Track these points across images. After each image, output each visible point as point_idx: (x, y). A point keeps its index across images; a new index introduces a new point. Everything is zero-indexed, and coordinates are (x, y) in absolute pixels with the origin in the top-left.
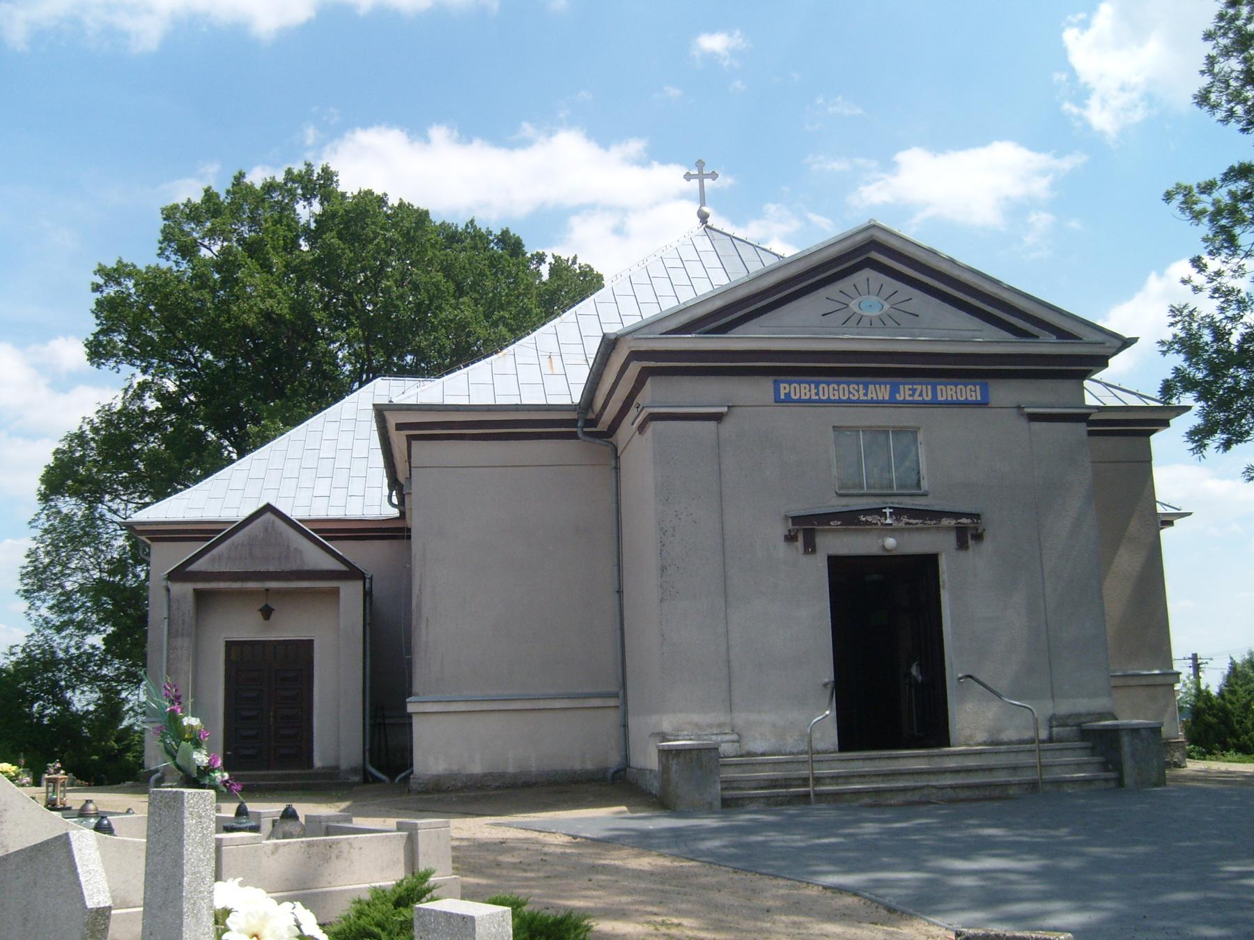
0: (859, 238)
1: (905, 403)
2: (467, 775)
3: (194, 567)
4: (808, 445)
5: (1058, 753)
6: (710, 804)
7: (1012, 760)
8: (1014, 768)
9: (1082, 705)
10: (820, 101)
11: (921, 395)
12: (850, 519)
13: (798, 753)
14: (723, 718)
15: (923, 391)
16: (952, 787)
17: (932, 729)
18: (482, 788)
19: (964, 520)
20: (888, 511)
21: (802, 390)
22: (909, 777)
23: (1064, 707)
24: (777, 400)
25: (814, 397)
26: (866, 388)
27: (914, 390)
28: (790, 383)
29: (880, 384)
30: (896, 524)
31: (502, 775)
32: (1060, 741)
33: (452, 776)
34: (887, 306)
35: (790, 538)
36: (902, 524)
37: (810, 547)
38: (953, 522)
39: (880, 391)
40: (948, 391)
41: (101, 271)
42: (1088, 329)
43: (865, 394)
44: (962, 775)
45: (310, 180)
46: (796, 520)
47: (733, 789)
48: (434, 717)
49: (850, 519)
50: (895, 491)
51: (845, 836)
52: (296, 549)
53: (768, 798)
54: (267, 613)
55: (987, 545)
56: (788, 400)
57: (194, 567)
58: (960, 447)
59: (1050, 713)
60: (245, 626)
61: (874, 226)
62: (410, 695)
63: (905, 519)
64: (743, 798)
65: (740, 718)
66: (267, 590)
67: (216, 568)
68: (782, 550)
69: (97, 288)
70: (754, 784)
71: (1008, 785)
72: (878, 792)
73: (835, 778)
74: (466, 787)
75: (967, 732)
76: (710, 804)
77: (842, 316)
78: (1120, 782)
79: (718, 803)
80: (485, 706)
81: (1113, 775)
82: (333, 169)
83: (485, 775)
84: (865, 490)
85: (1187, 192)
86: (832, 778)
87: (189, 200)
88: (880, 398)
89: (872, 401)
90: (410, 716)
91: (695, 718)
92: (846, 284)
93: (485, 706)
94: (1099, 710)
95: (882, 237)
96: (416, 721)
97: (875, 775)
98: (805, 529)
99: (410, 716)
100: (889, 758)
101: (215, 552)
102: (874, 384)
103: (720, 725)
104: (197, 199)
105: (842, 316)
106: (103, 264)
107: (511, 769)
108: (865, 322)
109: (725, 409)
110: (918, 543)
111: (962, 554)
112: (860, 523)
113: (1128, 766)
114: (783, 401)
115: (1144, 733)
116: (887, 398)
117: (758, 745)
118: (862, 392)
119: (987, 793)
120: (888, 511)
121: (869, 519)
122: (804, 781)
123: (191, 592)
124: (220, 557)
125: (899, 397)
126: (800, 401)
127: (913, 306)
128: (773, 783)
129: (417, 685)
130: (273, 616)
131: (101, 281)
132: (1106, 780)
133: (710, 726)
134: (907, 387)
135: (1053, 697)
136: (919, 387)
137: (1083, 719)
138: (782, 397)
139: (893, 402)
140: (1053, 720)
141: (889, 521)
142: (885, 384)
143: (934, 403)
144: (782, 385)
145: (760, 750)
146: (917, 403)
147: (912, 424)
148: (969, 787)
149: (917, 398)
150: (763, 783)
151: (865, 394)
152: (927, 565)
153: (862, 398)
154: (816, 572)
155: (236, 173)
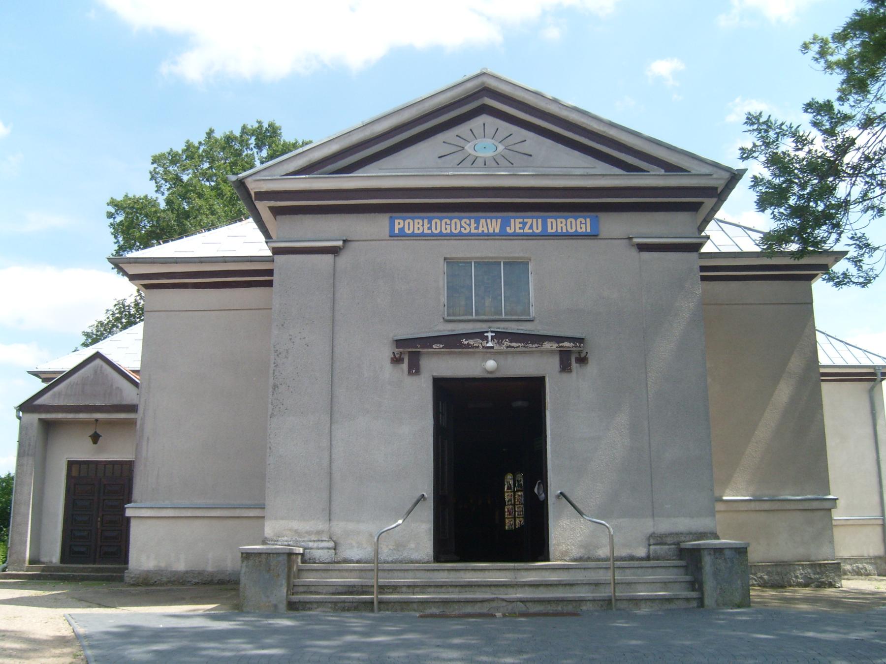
0: (470, 85)
1: (515, 236)
2: (171, 572)
3: (39, 402)
4: (408, 273)
5: (650, 570)
6: (276, 606)
7: (593, 576)
8: (597, 584)
9: (682, 524)
10: (738, 100)
11: (531, 227)
12: (452, 342)
13: (392, 562)
14: (321, 525)
15: (534, 224)
16: (523, 601)
17: (531, 543)
18: (183, 583)
19: (566, 344)
20: (490, 335)
21: (415, 225)
22: (488, 589)
23: (665, 526)
24: (392, 235)
25: (426, 231)
26: (477, 222)
27: (525, 224)
28: (404, 219)
29: (491, 219)
30: (497, 347)
31: (200, 573)
32: (658, 559)
33: (159, 572)
34: (501, 148)
35: (396, 360)
36: (503, 348)
37: (414, 368)
38: (555, 345)
39: (491, 224)
40: (558, 224)
41: (113, 203)
42: (696, 162)
43: (477, 228)
44: (541, 588)
45: (260, 133)
46: (399, 343)
47: (311, 593)
48: (149, 521)
49: (452, 342)
50: (503, 317)
51: (777, 635)
52: (118, 388)
53: (335, 603)
54: (95, 438)
55: (591, 368)
56: (402, 235)
57: (39, 402)
58: (570, 275)
59: (650, 530)
60: (82, 450)
61: (484, 74)
62: (129, 501)
63: (506, 343)
64: (311, 603)
65: (339, 527)
66: (97, 420)
67: (56, 403)
68: (388, 371)
69: (110, 215)
70: (331, 590)
71: (581, 601)
72: (445, 602)
73: (412, 587)
74: (170, 582)
75: (563, 548)
76: (276, 606)
77: (458, 157)
78: (701, 601)
79: (283, 606)
80: (189, 513)
81: (694, 594)
82: (277, 125)
83: (187, 572)
84: (474, 317)
85: (824, 42)
86: (409, 586)
87: (171, 150)
88: (491, 231)
89: (483, 235)
90: (128, 519)
91: (295, 525)
92: (463, 129)
93: (189, 513)
94: (702, 530)
95: (493, 84)
96: (133, 523)
97: (451, 586)
98: (410, 352)
99: (128, 519)
100: (474, 570)
101: (56, 389)
102: (486, 218)
103: (318, 533)
104: (179, 148)
105: (458, 157)
106: (115, 197)
107: (210, 569)
108: (480, 162)
109: (340, 243)
110: (522, 365)
111: (565, 376)
112: (462, 346)
113: (709, 584)
114: (397, 236)
115: (728, 553)
116: (497, 231)
117: (354, 553)
118: (473, 225)
119: (559, 608)
120: (490, 335)
121: (471, 342)
122: (382, 589)
123: (36, 422)
124: (60, 394)
125: (509, 230)
126: (413, 235)
127: (525, 148)
128: (351, 590)
129: (137, 493)
130: (99, 442)
131: (113, 210)
132: (687, 600)
133: (309, 533)
134: (518, 221)
135: (653, 516)
136: (529, 221)
137: (683, 538)
138: (397, 231)
139: (503, 235)
140: (657, 539)
141: (490, 344)
142: (497, 218)
143: (544, 235)
144: (397, 221)
145: (357, 558)
146: (527, 235)
147: (526, 255)
148: (548, 601)
149: (527, 230)
150: (341, 589)
151: (477, 228)
152: (534, 387)
153: (473, 231)
154: (420, 392)
155: (208, 131)
